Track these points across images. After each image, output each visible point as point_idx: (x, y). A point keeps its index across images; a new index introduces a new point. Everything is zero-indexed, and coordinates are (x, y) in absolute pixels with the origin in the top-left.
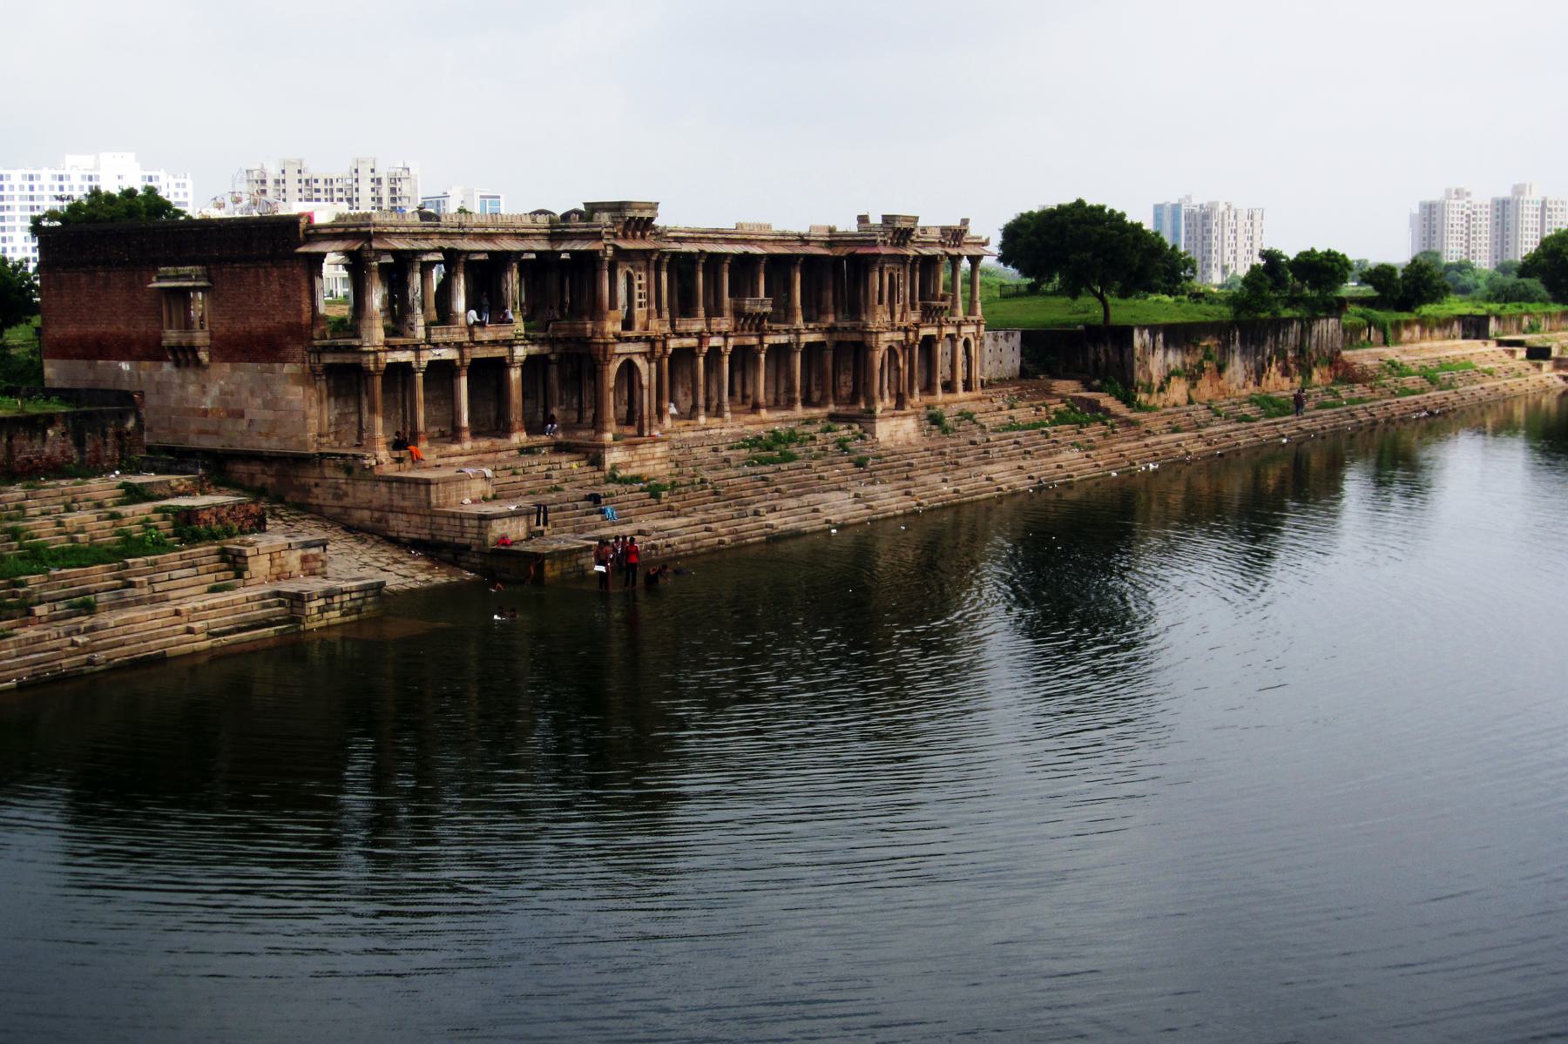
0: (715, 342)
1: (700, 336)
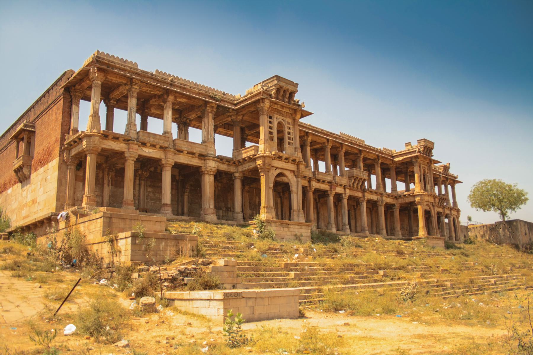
0: (339, 190)
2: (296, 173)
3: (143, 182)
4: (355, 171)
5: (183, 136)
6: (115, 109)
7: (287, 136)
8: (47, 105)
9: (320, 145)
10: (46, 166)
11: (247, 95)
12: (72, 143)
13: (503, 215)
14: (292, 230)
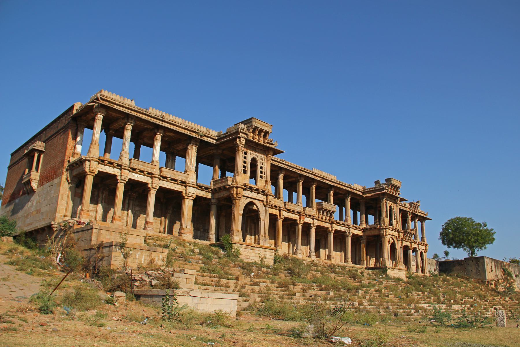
0: (308, 220)
1: (299, 213)
2: (266, 204)
3: (131, 202)
4: (325, 205)
5: (169, 164)
6: (113, 137)
7: (259, 170)
8: (56, 130)
9: (294, 179)
10: (51, 182)
11: (227, 133)
12: (75, 165)
13: (473, 253)
14: (257, 252)
